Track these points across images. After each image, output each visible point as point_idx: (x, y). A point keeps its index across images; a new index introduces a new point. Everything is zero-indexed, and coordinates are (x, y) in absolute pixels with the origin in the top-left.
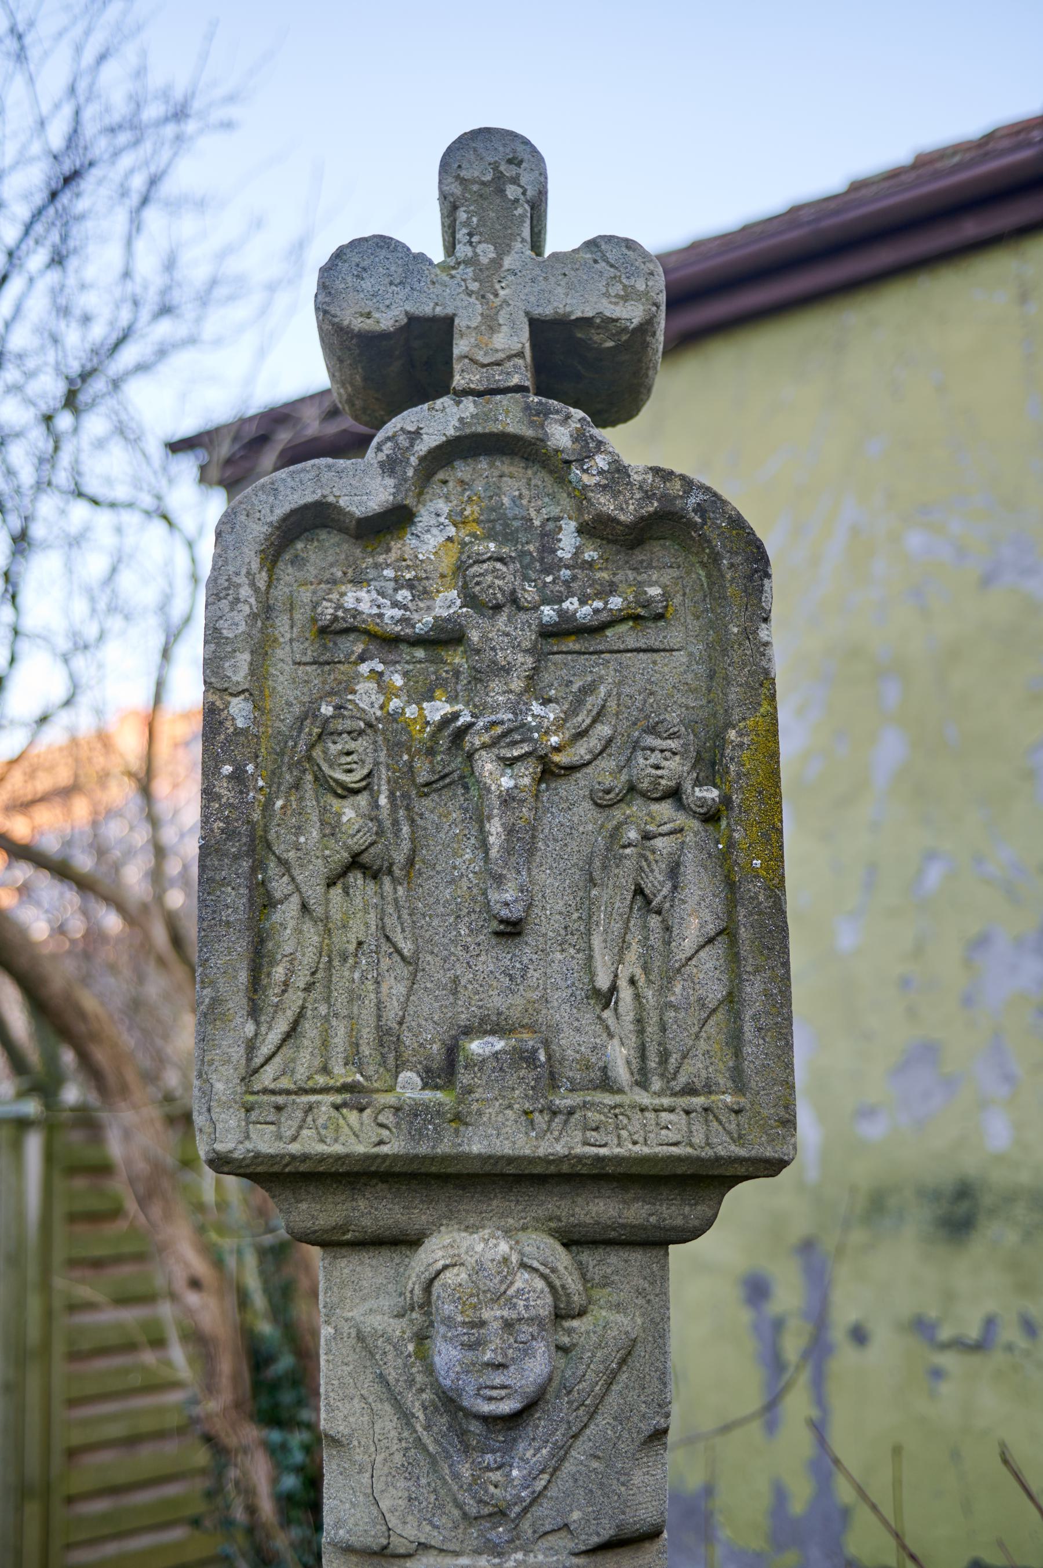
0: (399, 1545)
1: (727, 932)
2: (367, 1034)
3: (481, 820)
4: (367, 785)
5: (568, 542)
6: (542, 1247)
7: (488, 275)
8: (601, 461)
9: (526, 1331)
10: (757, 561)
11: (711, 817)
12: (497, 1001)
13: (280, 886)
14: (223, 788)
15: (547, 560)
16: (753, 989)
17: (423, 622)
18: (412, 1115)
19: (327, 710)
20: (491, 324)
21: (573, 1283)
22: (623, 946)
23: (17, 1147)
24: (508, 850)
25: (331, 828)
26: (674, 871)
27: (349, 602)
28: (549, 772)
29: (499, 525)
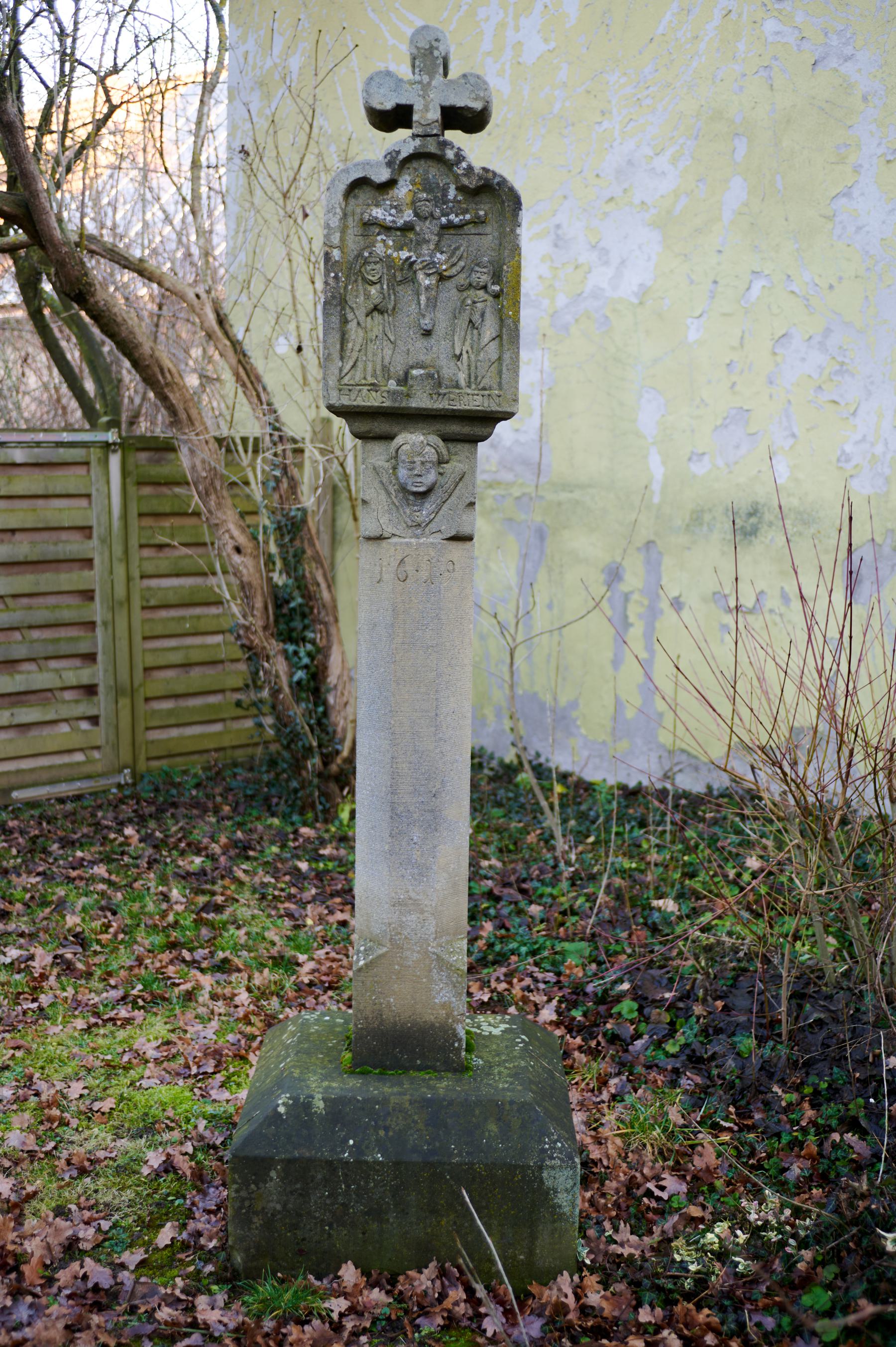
0: (386, 535)
1: (500, 336)
2: (379, 367)
3: (418, 294)
4: (380, 281)
5: (452, 193)
6: (435, 439)
7: (426, 87)
8: (464, 165)
9: (428, 465)
10: (516, 202)
11: (496, 296)
12: (422, 358)
13: (350, 316)
14: (331, 281)
15: (444, 200)
16: (507, 356)
17: (400, 222)
18: (393, 394)
19: (366, 254)
20: (426, 109)
21: (444, 451)
22: (465, 340)
23: (105, 462)
24: (427, 306)
25: (368, 296)
26: (483, 315)
27: (374, 213)
28: (442, 278)
29: (428, 186)
